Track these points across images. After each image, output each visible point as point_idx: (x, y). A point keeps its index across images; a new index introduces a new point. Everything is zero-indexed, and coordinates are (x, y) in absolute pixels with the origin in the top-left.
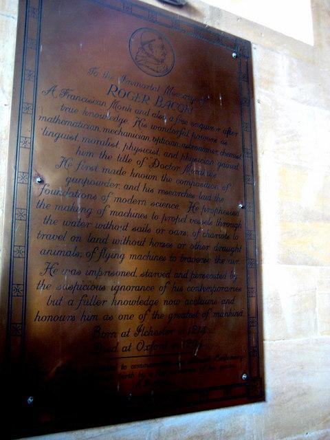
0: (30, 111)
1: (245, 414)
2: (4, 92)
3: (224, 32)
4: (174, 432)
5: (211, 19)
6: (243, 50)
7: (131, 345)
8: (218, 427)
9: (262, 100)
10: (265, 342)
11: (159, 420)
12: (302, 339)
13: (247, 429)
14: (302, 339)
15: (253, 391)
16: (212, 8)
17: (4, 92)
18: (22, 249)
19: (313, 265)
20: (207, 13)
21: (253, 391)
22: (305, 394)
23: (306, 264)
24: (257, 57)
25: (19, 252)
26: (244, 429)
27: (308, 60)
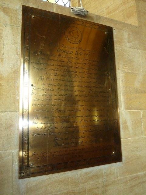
0: (28, 73)
1: (115, 166)
2: (17, 54)
3: (19, 163)
4: (96, 176)
5: (97, 20)
6: (110, 30)
7: (83, 140)
8: (104, 171)
9: (118, 48)
10: (121, 139)
11: (81, 170)
12: (136, 138)
13: (115, 172)
14: (136, 138)
15: (118, 158)
16: (97, 16)
17: (17, 54)
18: (27, 97)
19: (140, 110)
20: (95, 18)
21: (118, 158)
22: (138, 158)
23: (137, 109)
24: (115, 32)
25: (26, 98)
26: (114, 172)
27: (136, 32)
